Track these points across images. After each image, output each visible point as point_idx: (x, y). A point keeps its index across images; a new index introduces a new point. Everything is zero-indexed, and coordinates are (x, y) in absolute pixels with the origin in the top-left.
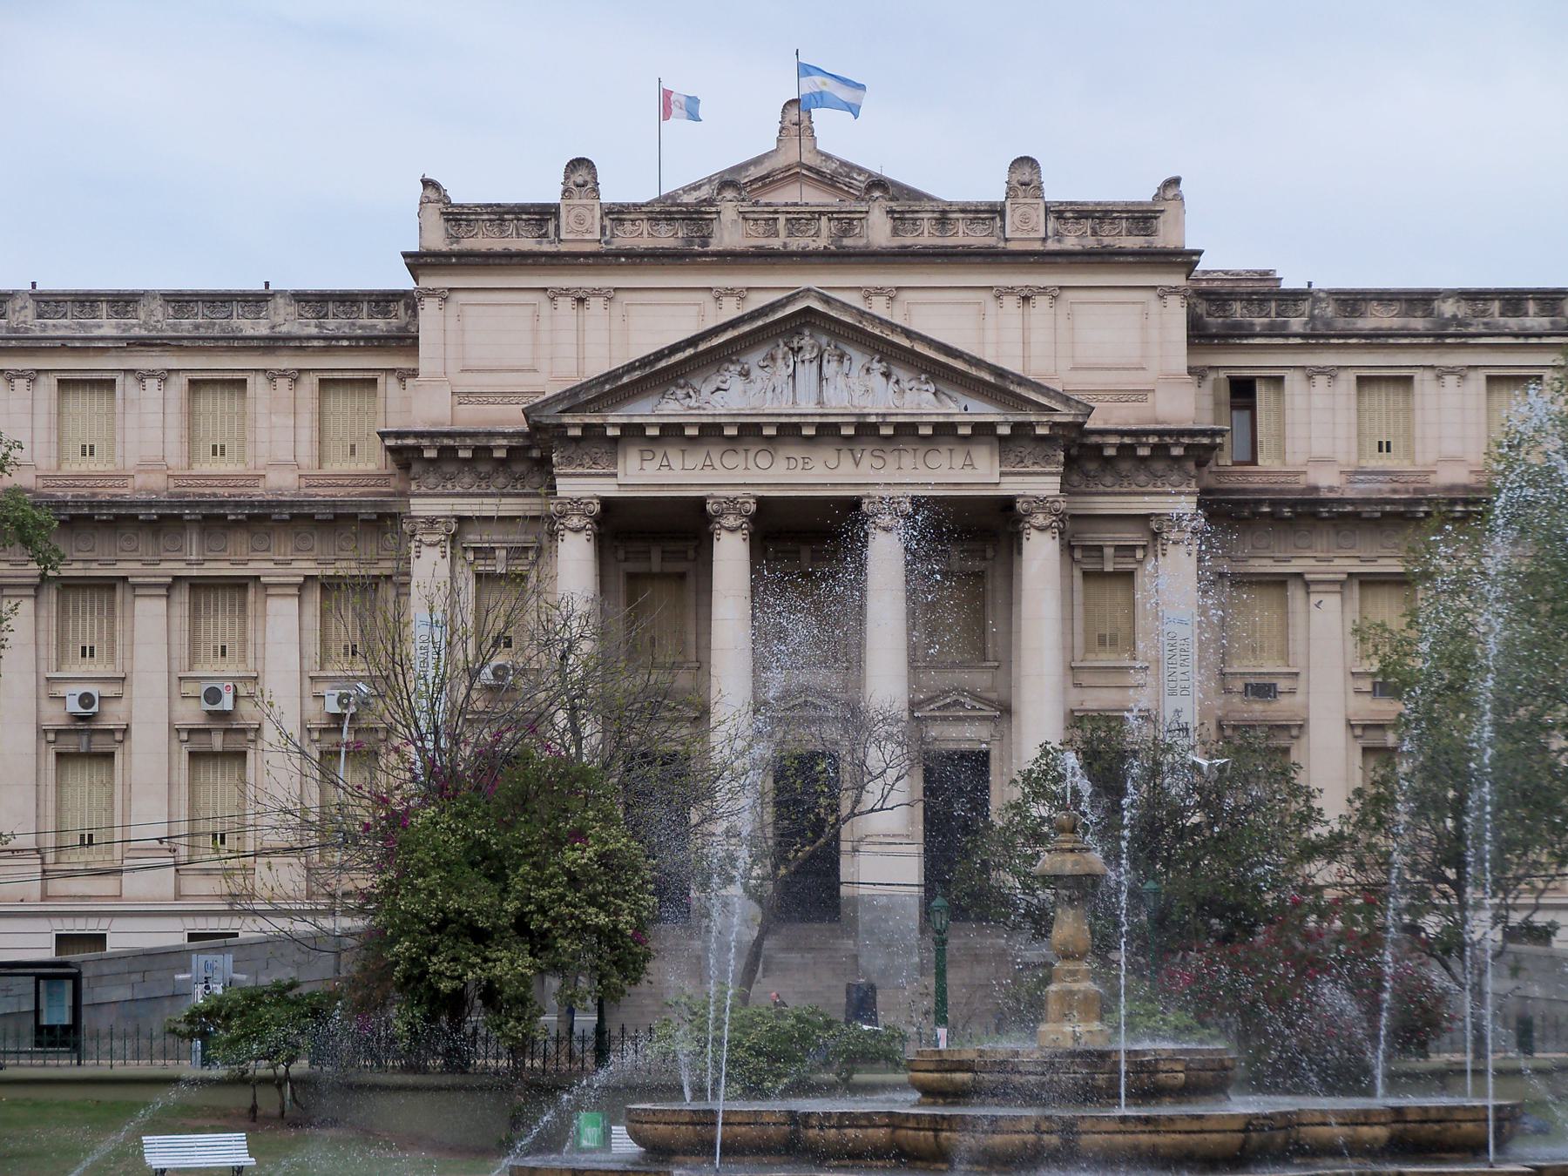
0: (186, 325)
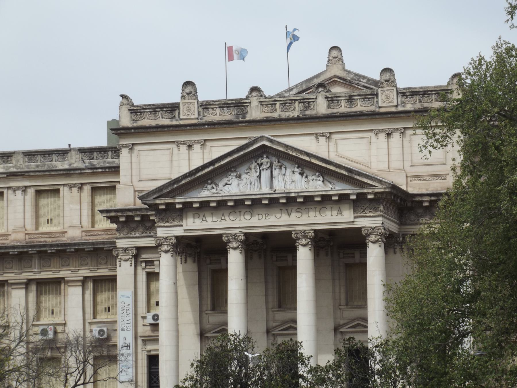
0: (33, 166)
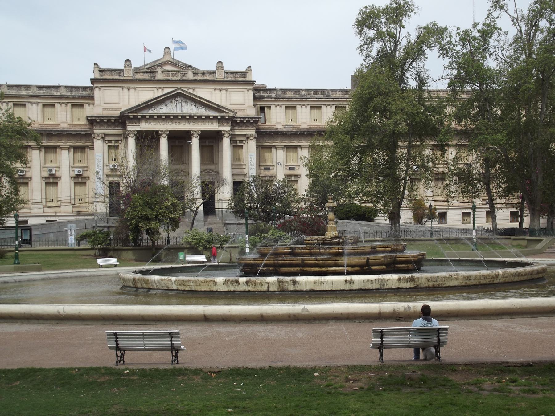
0: (41, 92)
